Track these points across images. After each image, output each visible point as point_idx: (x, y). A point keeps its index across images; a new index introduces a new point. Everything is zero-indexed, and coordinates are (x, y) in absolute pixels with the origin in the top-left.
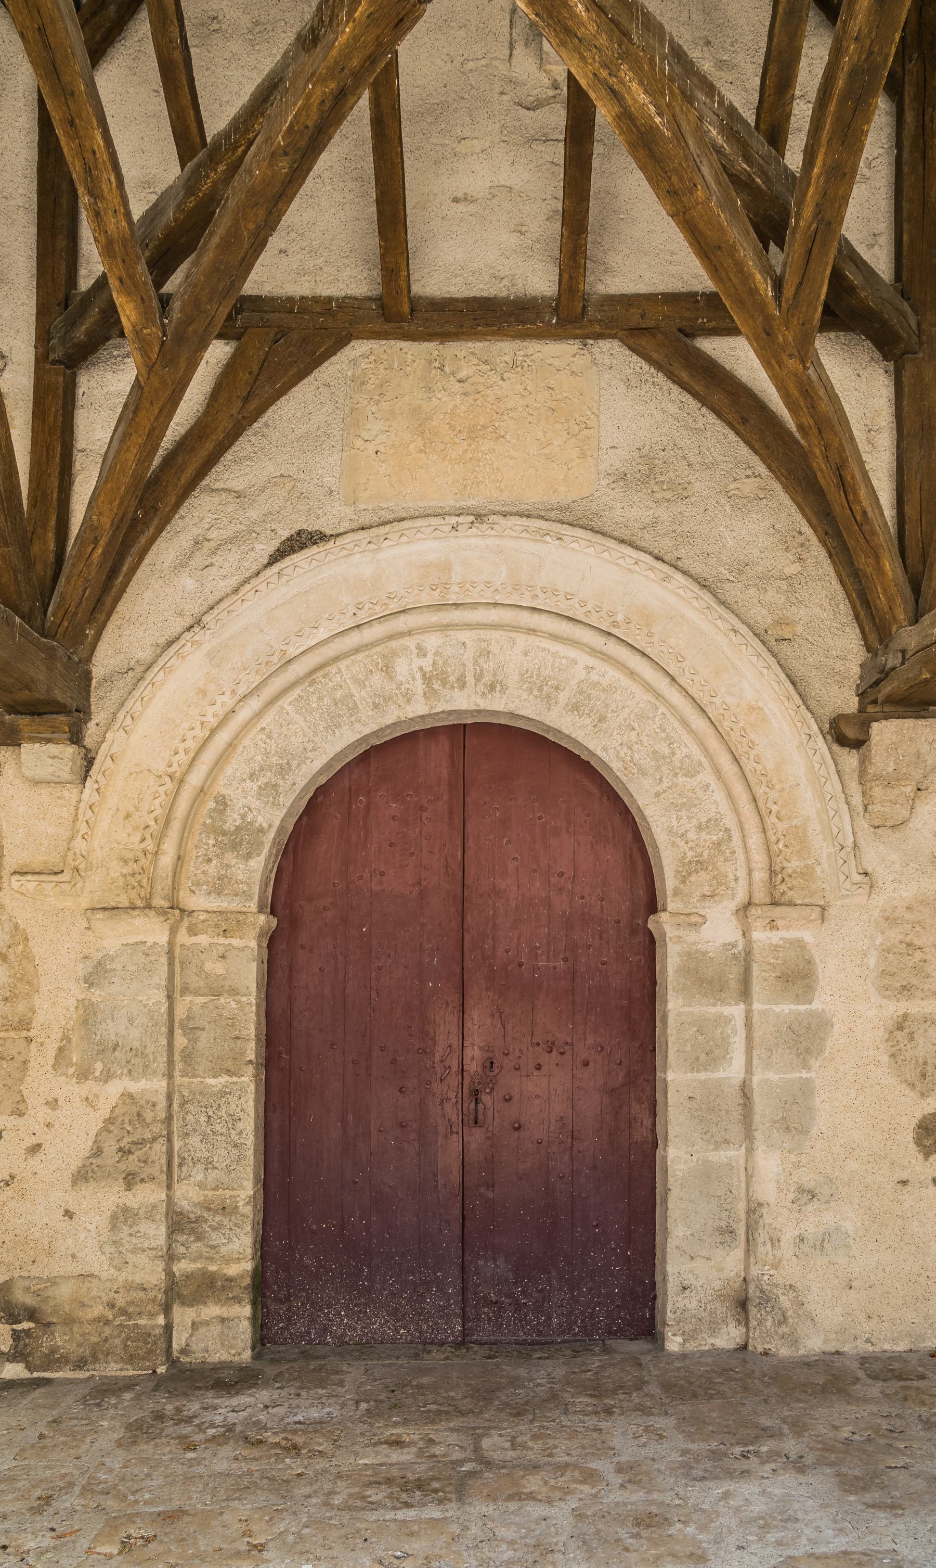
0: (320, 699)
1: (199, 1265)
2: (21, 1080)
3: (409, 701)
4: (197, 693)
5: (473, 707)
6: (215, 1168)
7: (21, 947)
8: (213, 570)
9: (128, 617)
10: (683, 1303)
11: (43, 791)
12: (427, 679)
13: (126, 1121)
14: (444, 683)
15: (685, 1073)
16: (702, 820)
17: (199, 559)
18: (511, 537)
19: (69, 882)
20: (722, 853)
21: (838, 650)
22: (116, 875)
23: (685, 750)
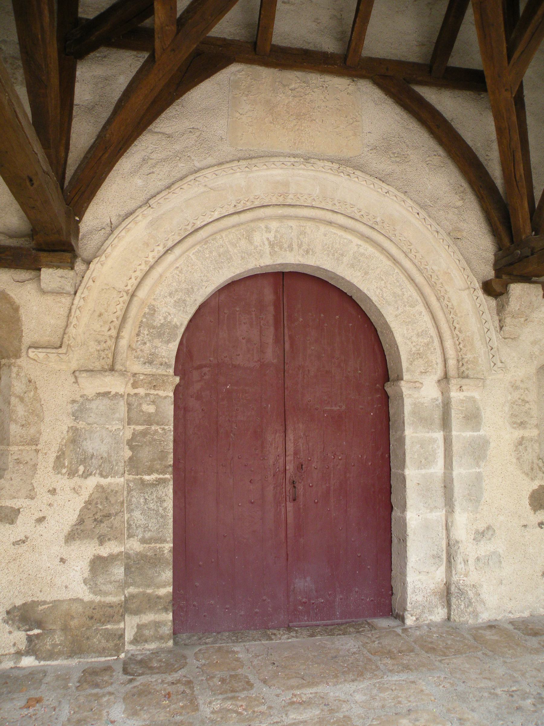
0: (211, 252)
1: (141, 590)
2: (33, 476)
3: (261, 256)
4: (143, 244)
5: (297, 262)
6: (150, 530)
7: (32, 393)
8: (154, 176)
9: (102, 199)
10: (415, 598)
11: (48, 298)
12: (272, 245)
13: (99, 502)
14: (281, 248)
15: (415, 470)
16: (419, 331)
17: (146, 169)
18: (322, 171)
19: (65, 354)
20: (429, 349)
21: (482, 246)
22: (93, 350)
23: (409, 293)
